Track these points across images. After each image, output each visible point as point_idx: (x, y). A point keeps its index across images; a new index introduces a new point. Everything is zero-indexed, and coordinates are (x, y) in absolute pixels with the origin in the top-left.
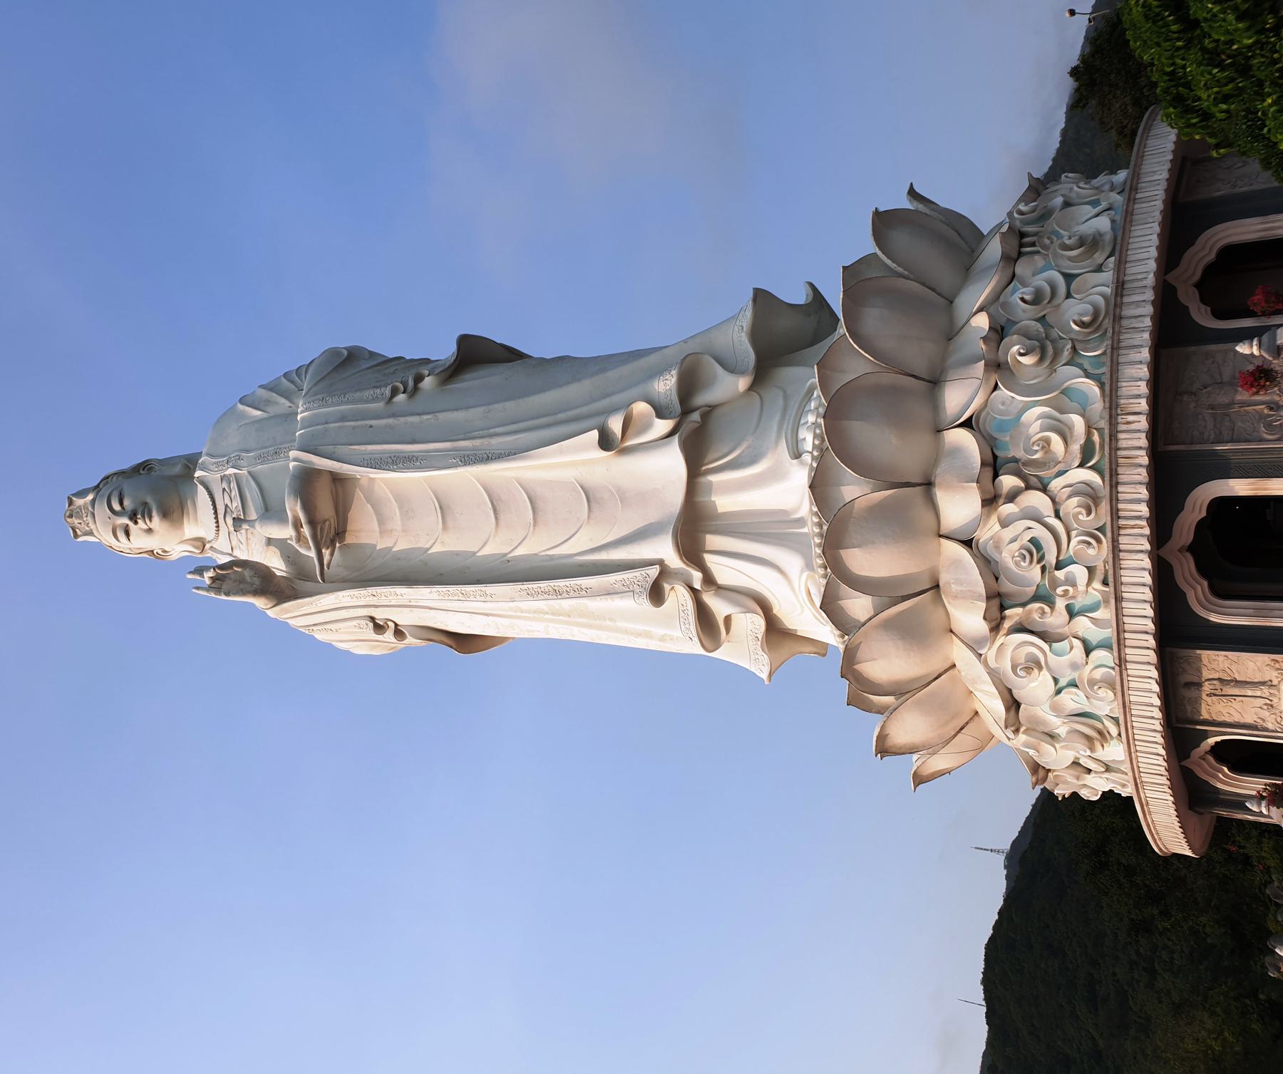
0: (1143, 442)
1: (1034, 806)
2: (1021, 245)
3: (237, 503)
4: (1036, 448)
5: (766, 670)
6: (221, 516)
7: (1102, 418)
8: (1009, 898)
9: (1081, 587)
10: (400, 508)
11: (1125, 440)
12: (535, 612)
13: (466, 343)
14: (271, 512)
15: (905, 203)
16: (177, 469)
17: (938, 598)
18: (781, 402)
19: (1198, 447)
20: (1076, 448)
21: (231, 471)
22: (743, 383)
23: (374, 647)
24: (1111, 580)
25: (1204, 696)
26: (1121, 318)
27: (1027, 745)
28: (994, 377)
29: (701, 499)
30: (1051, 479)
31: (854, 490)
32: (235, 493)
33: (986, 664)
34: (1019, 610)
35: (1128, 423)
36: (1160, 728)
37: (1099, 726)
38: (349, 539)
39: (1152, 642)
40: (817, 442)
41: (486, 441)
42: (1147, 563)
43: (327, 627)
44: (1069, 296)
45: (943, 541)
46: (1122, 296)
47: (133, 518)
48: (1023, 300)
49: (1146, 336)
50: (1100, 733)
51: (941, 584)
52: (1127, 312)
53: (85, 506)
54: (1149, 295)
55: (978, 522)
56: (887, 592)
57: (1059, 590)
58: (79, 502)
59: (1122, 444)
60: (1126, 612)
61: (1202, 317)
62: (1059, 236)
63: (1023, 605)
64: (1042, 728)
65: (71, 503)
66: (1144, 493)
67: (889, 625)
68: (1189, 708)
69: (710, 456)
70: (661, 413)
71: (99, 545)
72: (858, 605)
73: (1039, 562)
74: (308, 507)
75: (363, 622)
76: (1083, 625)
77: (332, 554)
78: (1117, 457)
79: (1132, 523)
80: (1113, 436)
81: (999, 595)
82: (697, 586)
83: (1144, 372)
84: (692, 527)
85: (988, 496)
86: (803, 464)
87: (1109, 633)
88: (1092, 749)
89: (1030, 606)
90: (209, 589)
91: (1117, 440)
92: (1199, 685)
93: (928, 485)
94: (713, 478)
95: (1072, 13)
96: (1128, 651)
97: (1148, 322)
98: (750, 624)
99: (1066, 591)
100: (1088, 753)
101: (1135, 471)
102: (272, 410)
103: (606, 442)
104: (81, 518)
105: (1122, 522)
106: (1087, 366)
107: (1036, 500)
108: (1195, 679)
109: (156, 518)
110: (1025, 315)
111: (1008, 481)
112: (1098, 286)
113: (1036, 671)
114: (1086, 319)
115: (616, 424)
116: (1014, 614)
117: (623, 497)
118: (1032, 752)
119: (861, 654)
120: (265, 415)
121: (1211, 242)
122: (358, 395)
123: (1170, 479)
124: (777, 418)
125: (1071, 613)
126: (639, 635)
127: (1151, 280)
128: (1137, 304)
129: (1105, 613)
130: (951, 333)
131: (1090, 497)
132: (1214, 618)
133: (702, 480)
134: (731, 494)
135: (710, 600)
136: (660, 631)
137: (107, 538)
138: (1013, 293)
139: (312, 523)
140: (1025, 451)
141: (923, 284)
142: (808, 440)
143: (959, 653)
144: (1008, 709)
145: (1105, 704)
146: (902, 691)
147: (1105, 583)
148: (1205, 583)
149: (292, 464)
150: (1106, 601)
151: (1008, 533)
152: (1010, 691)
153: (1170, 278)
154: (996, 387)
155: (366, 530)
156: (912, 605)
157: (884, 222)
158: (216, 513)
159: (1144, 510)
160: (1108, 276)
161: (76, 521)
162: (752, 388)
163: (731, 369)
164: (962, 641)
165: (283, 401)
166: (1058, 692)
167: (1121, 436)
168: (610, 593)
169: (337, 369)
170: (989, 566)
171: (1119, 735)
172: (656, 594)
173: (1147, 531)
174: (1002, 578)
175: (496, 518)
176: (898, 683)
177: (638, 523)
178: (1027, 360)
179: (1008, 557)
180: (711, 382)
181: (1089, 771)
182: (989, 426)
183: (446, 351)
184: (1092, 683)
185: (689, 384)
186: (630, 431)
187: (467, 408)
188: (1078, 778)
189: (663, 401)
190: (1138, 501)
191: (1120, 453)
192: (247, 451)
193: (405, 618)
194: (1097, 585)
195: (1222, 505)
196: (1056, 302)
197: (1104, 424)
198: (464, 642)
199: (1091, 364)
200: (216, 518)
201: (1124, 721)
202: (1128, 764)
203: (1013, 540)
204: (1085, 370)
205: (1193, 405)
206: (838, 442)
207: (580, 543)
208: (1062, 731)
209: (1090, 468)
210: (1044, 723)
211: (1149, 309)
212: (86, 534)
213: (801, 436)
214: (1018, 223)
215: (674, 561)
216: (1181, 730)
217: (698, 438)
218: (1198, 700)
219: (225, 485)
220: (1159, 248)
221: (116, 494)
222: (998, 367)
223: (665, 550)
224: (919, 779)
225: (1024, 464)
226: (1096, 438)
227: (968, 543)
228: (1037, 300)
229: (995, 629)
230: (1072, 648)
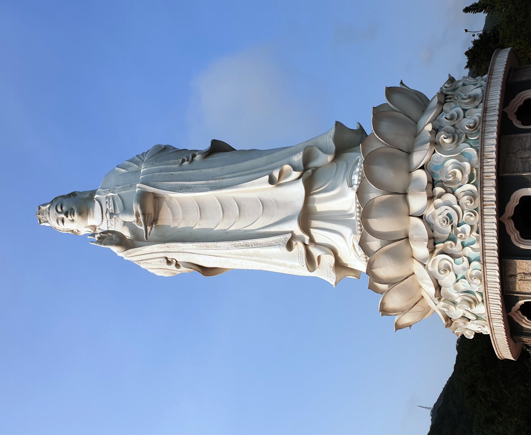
0: (494, 170)
1: (444, 389)
2: (446, 99)
3: (112, 208)
4: (450, 176)
5: (334, 280)
6: (104, 214)
7: (477, 164)
8: (432, 428)
9: (468, 234)
10: (182, 209)
11: (486, 169)
12: (237, 255)
13: (214, 142)
14: (126, 210)
15: (398, 85)
16: (87, 196)
17: (408, 243)
18: (345, 165)
19: (516, 174)
20: (466, 176)
21: (111, 194)
22: (330, 158)
23: (166, 272)
24: (480, 231)
25: (517, 281)
26: (485, 121)
27: (443, 307)
28: (434, 148)
29: (310, 205)
30: (457, 185)
31: (375, 194)
32: (111, 203)
33: (427, 269)
34: (442, 245)
35: (488, 162)
36: (499, 292)
37: (474, 297)
38: (159, 223)
39: (496, 254)
40: (360, 178)
41: (221, 180)
42: (495, 220)
43: (146, 261)
44: (464, 117)
45: (411, 217)
46: (486, 113)
47: (66, 214)
48: (446, 118)
49: (495, 128)
50: (475, 301)
51: (409, 236)
52: (488, 119)
53: (46, 210)
54: (497, 112)
55: (425, 208)
56: (387, 238)
57: (459, 235)
58: (43, 208)
59: (485, 171)
60: (486, 241)
61: (518, 125)
62: (460, 95)
63: (443, 242)
64: (452, 300)
65: (39, 208)
66: (494, 191)
67: (387, 252)
68: (511, 286)
69: (315, 187)
70: (295, 169)
71: (51, 228)
72: (375, 244)
73: (450, 224)
74: (143, 207)
75: (162, 259)
76: (468, 251)
77: (151, 229)
78: (483, 176)
79: (489, 203)
80: (482, 168)
81: (434, 238)
82: (307, 243)
83: (494, 142)
84: (306, 217)
85: (430, 196)
86: (353, 189)
87: (479, 254)
88: (471, 308)
89: (446, 243)
90: (97, 242)
91: (483, 169)
92: (515, 276)
93: (405, 194)
94: (316, 196)
95: (466, 31)
96: (487, 258)
97: (496, 123)
98: (328, 260)
99: (461, 236)
100: (469, 309)
101: (490, 182)
102: (130, 169)
103: (271, 181)
104: (43, 215)
105: (485, 203)
106: (471, 144)
107: (450, 197)
108: (514, 273)
109: (76, 215)
110: (447, 125)
111: (438, 190)
112: (477, 113)
113: (448, 271)
114: (471, 125)
115: (276, 174)
116: (440, 246)
117: (278, 204)
118: (445, 310)
119: (375, 264)
120: (127, 171)
121: (521, 98)
122: (168, 161)
123: (505, 187)
124: (342, 175)
125: (463, 246)
126: (280, 265)
127: (497, 107)
128: (492, 116)
129: (477, 246)
130: (416, 134)
131: (472, 196)
132: (522, 247)
133: (311, 197)
134: (323, 203)
135: (312, 249)
136: (289, 263)
137: (53, 223)
138: (442, 116)
139: (144, 214)
140: (446, 177)
141: (406, 115)
142: (356, 178)
143: (417, 267)
144: (436, 289)
145: (477, 286)
146: (392, 283)
147: (478, 232)
148: (518, 232)
149: (137, 190)
150: (478, 240)
151: (438, 212)
152: (437, 281)
153: (505, 110)
154: (434, 152)
155: (167, 219)
156: (397, 244)
157: (390, 91)
158: (102, 212)
159: (494, 198)
160: (480, 109)
161: (41, 216)
162: (333, 160)
163: (325, 152)
164: (418, 261)
165: (135, 165)
166: (457, 281)
167: (485, 167)
168: (270, 245)
169: (159, 152)
170: (430, 226)
171: (483, 301)
172: (289, 246)
173: (495, 207)
174: (435, 231)
175: (223, 214)
176: (390, 279)
177: (283, 216)
178: (447, 141)
179: (438, 222)
180: (317, 157)
181: (469, 320)
182: (430, 167)
183: (206, 146)
184: (471, 276)
185: (307, 159)
186: (282, 178)
187: (214, 167)
188: (465, 324)
189: (296, 165)
190: (492, 194)
191: (485, 174)
192: (118, 186)
193: (181, 258)
194: (474, 233)
195: (525, 200)
196: (459, 119)
197: (478, 166)
198: (205, 270)
199: (473, 143)
200: (102, 214)
201: (484, 294)
202: (487, 320)
203: (440, 214)
204: (471, 145)
205: (514, 158)
206: (368, 174)
207: (258, 224)
208: (458, 300)
209: (472, 184)
210: (451, 296)
211: (497, 118)
212: (45, 222)
213: (353, 178)
214: (444, 92)
215: (298, 232)
216: (508, 297)
217: (310, 179)
218: (515, 282)
219: (107, 200)
220: (500, 100)
221: (60, 204)
222: (435, 144)
223: (294, 227)
224: (398, 327)
225: (445, 183)
226: (475, 172)
227: (421, 217)
228: (452, 118)
229: (432, 252)
230: (463, 261)
